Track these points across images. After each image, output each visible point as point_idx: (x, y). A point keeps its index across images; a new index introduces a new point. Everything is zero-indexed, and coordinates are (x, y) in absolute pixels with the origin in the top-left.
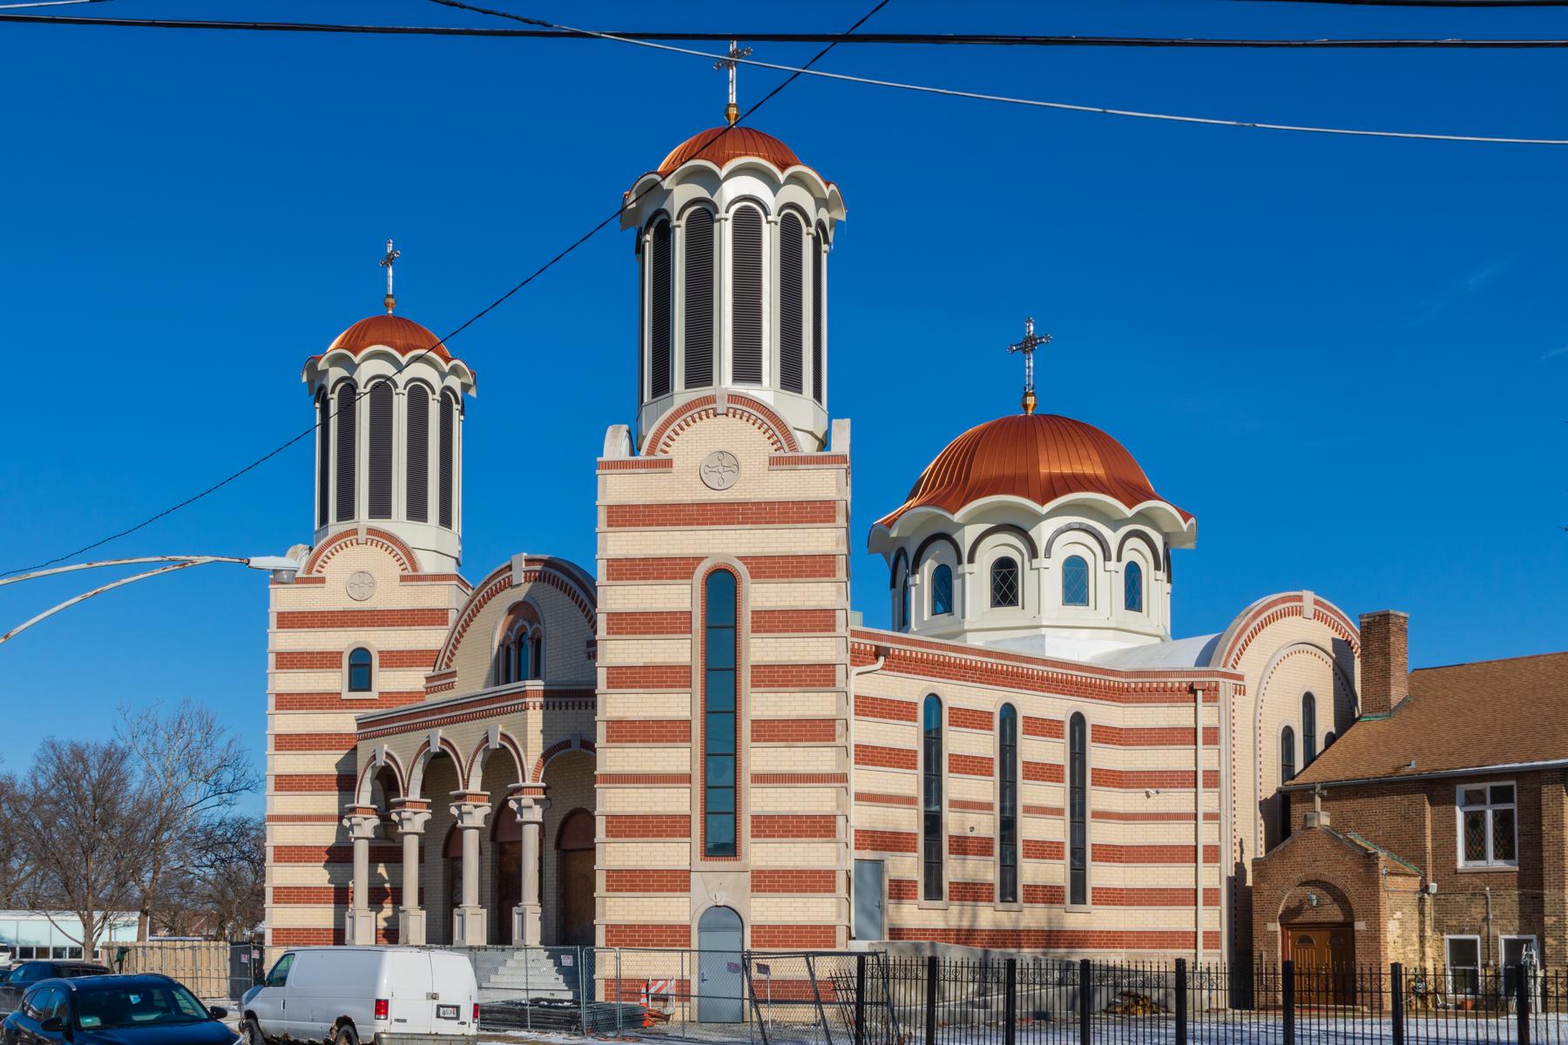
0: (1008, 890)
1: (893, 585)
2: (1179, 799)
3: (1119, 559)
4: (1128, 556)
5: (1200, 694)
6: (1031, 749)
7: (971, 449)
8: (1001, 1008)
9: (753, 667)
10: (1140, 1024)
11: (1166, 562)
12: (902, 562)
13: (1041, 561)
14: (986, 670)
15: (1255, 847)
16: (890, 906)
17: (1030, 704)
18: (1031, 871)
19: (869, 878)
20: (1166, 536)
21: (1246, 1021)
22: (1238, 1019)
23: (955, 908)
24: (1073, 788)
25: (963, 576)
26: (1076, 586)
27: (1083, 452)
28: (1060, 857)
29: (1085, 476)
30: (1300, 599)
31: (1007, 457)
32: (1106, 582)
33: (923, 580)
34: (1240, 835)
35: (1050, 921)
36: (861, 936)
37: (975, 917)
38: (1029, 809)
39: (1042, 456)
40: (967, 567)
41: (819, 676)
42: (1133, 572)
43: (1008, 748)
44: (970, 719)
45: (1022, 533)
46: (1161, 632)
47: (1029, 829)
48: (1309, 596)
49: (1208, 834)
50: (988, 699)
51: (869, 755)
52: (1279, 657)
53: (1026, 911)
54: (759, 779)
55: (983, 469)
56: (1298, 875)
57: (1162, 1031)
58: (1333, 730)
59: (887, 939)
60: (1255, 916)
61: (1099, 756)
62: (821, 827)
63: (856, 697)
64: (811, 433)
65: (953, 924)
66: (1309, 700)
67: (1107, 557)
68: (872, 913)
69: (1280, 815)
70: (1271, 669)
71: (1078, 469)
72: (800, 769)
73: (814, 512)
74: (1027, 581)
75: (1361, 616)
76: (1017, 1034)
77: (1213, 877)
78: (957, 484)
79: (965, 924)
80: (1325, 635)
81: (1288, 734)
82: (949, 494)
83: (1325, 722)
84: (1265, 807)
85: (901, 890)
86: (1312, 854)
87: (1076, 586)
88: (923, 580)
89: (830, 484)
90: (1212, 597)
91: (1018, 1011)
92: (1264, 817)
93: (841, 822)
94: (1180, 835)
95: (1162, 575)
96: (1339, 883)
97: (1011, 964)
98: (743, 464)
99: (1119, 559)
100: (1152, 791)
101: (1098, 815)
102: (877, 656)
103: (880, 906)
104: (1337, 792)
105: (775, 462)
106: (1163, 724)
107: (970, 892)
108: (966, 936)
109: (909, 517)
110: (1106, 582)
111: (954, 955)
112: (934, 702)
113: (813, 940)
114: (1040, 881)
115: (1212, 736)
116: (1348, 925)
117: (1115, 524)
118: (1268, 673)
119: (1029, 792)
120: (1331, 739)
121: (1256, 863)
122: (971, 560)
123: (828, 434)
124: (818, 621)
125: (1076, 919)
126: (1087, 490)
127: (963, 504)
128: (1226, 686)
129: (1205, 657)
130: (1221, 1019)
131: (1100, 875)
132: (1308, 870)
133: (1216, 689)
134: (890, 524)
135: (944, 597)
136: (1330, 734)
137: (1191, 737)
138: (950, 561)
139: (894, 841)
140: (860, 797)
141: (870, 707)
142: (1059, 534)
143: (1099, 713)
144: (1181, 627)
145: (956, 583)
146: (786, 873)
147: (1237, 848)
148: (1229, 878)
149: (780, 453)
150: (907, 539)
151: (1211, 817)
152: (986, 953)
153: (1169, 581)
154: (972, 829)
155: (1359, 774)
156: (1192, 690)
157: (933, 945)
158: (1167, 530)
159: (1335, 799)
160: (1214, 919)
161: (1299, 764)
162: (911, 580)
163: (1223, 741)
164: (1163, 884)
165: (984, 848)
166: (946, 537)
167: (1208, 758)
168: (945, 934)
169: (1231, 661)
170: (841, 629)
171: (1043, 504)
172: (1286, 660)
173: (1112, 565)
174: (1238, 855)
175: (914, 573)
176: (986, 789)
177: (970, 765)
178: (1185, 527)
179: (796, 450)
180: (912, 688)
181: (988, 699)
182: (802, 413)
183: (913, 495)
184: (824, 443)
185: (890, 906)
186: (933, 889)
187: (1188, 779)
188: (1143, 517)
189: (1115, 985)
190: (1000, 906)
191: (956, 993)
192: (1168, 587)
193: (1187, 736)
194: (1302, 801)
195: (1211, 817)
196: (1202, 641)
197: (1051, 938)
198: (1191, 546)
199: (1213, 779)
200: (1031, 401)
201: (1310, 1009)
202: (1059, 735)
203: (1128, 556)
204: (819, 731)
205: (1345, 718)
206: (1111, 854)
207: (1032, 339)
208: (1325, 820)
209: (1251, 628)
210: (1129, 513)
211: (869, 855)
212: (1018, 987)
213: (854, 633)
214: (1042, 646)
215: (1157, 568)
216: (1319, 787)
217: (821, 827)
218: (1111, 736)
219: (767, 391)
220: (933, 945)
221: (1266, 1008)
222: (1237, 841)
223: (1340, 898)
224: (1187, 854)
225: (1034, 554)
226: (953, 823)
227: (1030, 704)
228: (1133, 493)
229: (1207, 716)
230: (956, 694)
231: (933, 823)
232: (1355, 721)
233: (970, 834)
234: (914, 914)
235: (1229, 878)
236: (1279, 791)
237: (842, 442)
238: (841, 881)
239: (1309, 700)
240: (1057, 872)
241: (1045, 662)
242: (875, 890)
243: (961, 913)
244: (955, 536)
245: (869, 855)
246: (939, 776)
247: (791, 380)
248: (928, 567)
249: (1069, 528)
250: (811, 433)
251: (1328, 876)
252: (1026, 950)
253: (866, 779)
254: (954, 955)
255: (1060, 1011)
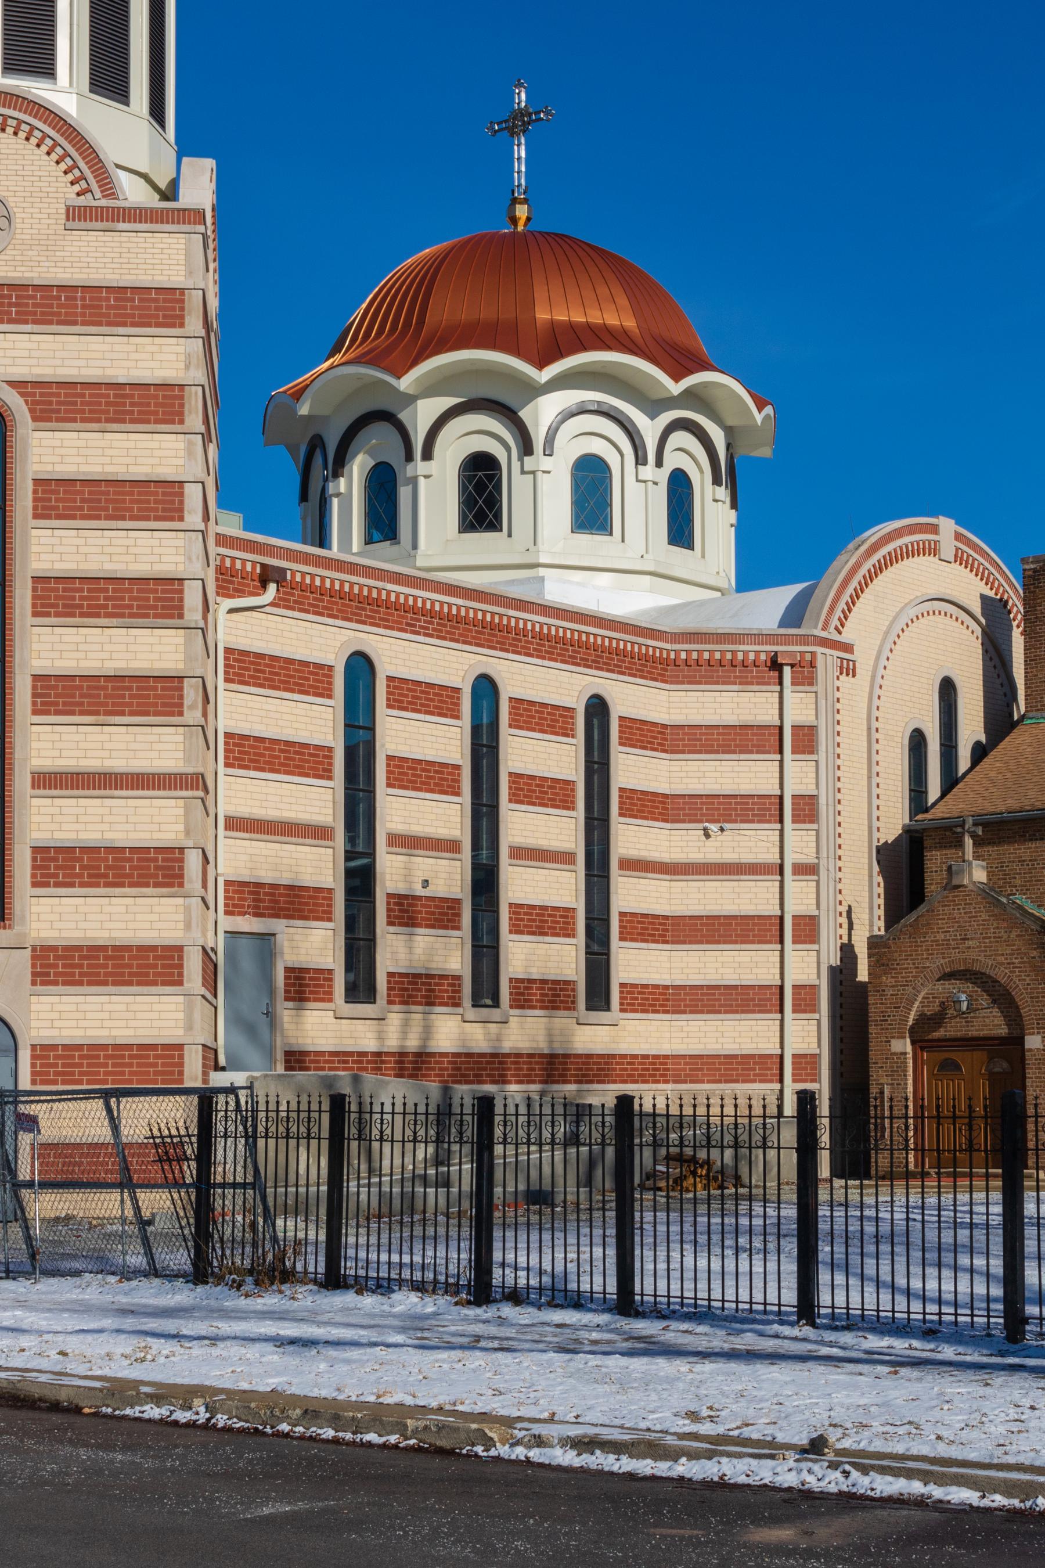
0: (486, 985)
1: (304, 497)
2: (753, 842)
3: (659, 463)
4: (673, 460)
5: (787, 670)
6: (523, 753)
7: (426, 281)
8: (466, 1187)
9: (36, 579)
10: (702, 1209)
11: (729, 474)
12: (318, 458)
13: (538, 461)
14: (450, 617)
15: (869, 921)
16: (286, 1013)
17: (522, 678)
18: (522, 956)
19: (248, 965)
20: (729, 431)
21: (870, 1200)
22: (854, 1196)
23: (395, 1019)
24: (589, 819)
25: (414, 481)
26: (592, 501)
27: (603, 291)
28: (568, 932)
29: (606, 328)
30: (934, 529)
31: (488, 293)
32: (639, 500)
33: (351, 487)
34: (848, 899)
35: (550, 1038)
36: (235, 1064)
37: (427, 1032)
38: (520, 853)
39: (540, 294)
40: (421, 467)
41: (151, 599)
42: (679, 487)
43: (485, 748)
44: (424, 698)
45: (508, 414)
46: (723, 584)
47: (520, 885)
48: (947, 526)
49: (800, 898)
50: (451, 665)
51: (252, 753)
52: (904, 620)
53: (514, 1022)
54: (49, 781)
55: (444, 310)
56: (939, 963)
57: (744, 1221)
58: (983, 738)
59: (280, 1069)
60: (872, 1029)
61: (632, 769)
62: (155, 868)
63: (228, 650)
64: (145, 177)
65: (392, 1043)
66: (948, 689)
67: (640, 460)
68: (256, 1026)
69: (907, 869)
70: (892, 638)
71: (595, 317)
72: (118, 764)
73: (148, 308)
74: (516, 491)
75: (1024, 561)
76: (497, 1234)
77: (806, 966)
78: (406, 331)
79: (413, 1043)
80: (970, 589)
81: (917, 741)
82: (389, 350)
83: (971, 728)
84: (885, 855)
85: (304, 986)
86: (957, 930)
87: (592, 501)
88: (351, 487)
89: (173, 259)
90: (798, 524)
91: (498, 1190)
92: (883, 872)
93: (193, 862)
94: (754, 898)
95: (722, 493)
96: (1001, 974)
97: (485, 1106)
98: (18, 216)
99: (659, 463)
100: (713, 827)
101: (631, 865)
102: (264, 583)
103: (270, 1015)
104: (998, 830)
105: (76, 215)
106: (729, 718)
107: (420, 989)
108: (413, 1064)
109: (329, 383)
110: (639, 500)
111: (392, 1093)
112: (360, 666)
113: (142, 1069)
114: (535, 974)
115: (806, 740)
116: (1016, 1041)
117: (653, 406)
118: (889, 645)
119: (520, 824)
120: (980, 752)
121: (874, 943)
122: (427, 455)
123: (174, 184)
124: (151, 501)
125: (592, 1036)
126: (609, 348)
127: (415, 363)
128: (827, 660)
129: (794, 615)
130: (963, 1234)
131: (633, 963)
132: (955, 955)
133: (812, 665)
134: (298, 395)
135: (384, 519)
136: (978, 744)
137: (774, 740)
138: (394, 457)
139: (293, 902)
140: (237, 824)
141: (253, 669)
142: (565, 419)
143: (632, 698)
144: (750, 576)
145: (404, 493)
146: (94, 951)
147: (844, 920)
148: (832, 969)
149: (86, 200)
150: (325, 419)
151: (806, 870)
152: (446, 1091)
153: (734, 505)
154: (426, 883)
155: (1027, 804)
156: (775, 665)
157: (356, 1080)
158: (730, 422)
159: (991, 843)
160: (807, 1035)
161: (934, 791)
162: (331, 487)
163: (822, 748)
164: (730, 978)
165: (441, 914)
166: (387, 417)
167: (800, 776)
168: (377, 1060)
169: (835, 622)
170: (193, 518)
171: (541, 365)
172: (913, 622)
173: (648, 471)
174: (844, 931)
175: (336, 475)
176: (448, 816)
177: (422, 776)
178: (759, 418)
179: (113, 196)
180: (325, 642)
181: (451, 665)
182: (129, 138)
183: (336, 349)
184: (170, 193)
185: (286, 1013)
186: (361, 987)
187: (769, 809)
188: (693, 398)
189: (655, 1144)
190: (471, 1013)
191: (397, 1159)
192: (732, 516)
193: (765, 739)
194: (942, 846)
195: (806, 870)
196: (784, 595)
197: (553, 1066)
198: (766, 452)
199: (807, 809)
200: (522, 212)
201: (955, 1176)
202: (567, 732)
203: (673, 460)
204: (150, 697)
205: (1000, 722)
206: (651, 929)
207: (522, 113)
208: (980, 875)
209: (863, 571)
210: (675, 388)
211: (247, 924)
212: (498, 1149)
213: (222, 540)
214: (541, 592)
215: (717, 481)
216: (970, 821)
217: (155, 868)
218: (649, 736)
219: (66, 90)
220: (356, 1080)
221: (890, 1176)
222: (844, 909)
223: (1003, 998)
224: (768, 930)
225: (527, 448)
226: (393, 872)
227: (522, 678)
228: (681, 361)
229: (799, 708)
230: (398, 655)
231: (360, 879)
232: (1013, 725)
233: (419, 891)
234: (325, 1027)
235: (832, 969)
236: (907, 831)
237: (200, 185)
238: (193, 966)
239: (948, 689)
240: (563, 958)
241: (545, 609)
242: (257, 984)
243: (406, 1025)
244: (403, 416)
245: (247, 924)
246: (371, 792)
247: (108, 78)
248: (359, 467)
249: (582, 410)
250: (145, 177)
251: (985, 963)
252: (513, 1087)
253: (243, 793)
254: (392, 1093)
255: (570, 1190)
